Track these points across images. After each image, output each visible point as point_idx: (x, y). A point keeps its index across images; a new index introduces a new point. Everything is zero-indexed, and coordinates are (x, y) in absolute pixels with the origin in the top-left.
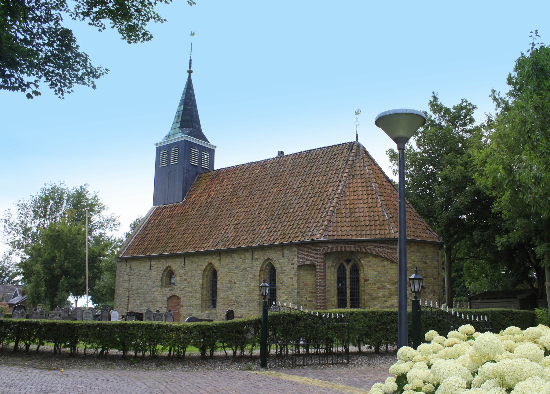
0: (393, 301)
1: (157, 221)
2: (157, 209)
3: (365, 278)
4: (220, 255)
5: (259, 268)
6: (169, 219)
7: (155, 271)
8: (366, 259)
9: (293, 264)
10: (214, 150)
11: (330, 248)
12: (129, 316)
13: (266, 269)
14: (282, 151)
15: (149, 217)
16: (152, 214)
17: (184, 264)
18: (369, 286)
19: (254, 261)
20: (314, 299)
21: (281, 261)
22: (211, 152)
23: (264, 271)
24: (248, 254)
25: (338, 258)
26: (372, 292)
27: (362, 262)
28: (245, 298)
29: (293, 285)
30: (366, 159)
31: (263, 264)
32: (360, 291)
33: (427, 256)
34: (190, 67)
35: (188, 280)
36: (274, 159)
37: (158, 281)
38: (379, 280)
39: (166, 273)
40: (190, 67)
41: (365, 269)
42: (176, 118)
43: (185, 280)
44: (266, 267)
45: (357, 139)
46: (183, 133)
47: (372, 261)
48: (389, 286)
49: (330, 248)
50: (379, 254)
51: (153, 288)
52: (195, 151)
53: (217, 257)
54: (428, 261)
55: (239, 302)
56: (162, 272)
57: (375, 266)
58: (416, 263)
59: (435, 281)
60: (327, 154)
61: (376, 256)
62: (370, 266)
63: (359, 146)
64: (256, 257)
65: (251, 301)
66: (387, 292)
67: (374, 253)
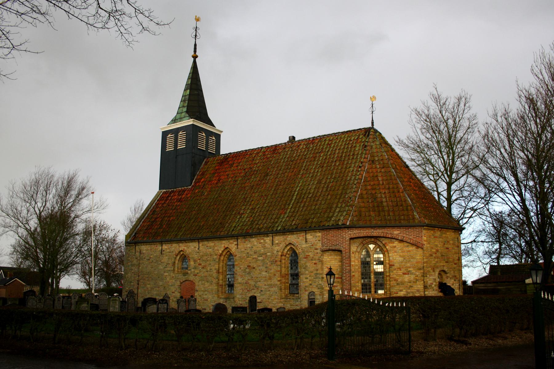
1: (165, 205)
2: (164, 193)
3: (391, 264)
5: (280, 254)
6: (179, 204)
7: (166, 256)
8: (391, 245)
9: (317, 249)
10: (220, 135)
12: (161, 303)
13: (287, 254)
14: (293, 137)
15: (156, 201)
16: (159, 197)
17: (198, 249)
18: (395, 272)
19: (274, 246)
20: (338, 284)
22: (218, 137)
23: (285, 256)
24: (268, 238)
25: (363, 244)
26: (398, 278)
27: (387, 247)
28: (265, 283)
30: (384, 145)
31: (284, 250)
33: (448, 242)
34: (195, 51)
35: (202, 265)
36: (285, 143)
37: (171, 265)
38: (405, 265)
39: (178, 257)
40: (195, 51)
41: (390, 255)
42: (182, 103)
43: (200, 264)
44: (287, 251)
46: (190, 117)
47: (397, 247)
48: (414, 271)
50: (404, 239)
51: (165, 272)
53: (234, 241)
55: (259, 287)
58: (439, 248)
59: (455, 266)
60: (342, 139)
61: (401, 241)
62: (395, 252)
63: (376, 131)
64: (277, 242)
65: (271, 286)
66: (412, 277)
67: (400, 239)
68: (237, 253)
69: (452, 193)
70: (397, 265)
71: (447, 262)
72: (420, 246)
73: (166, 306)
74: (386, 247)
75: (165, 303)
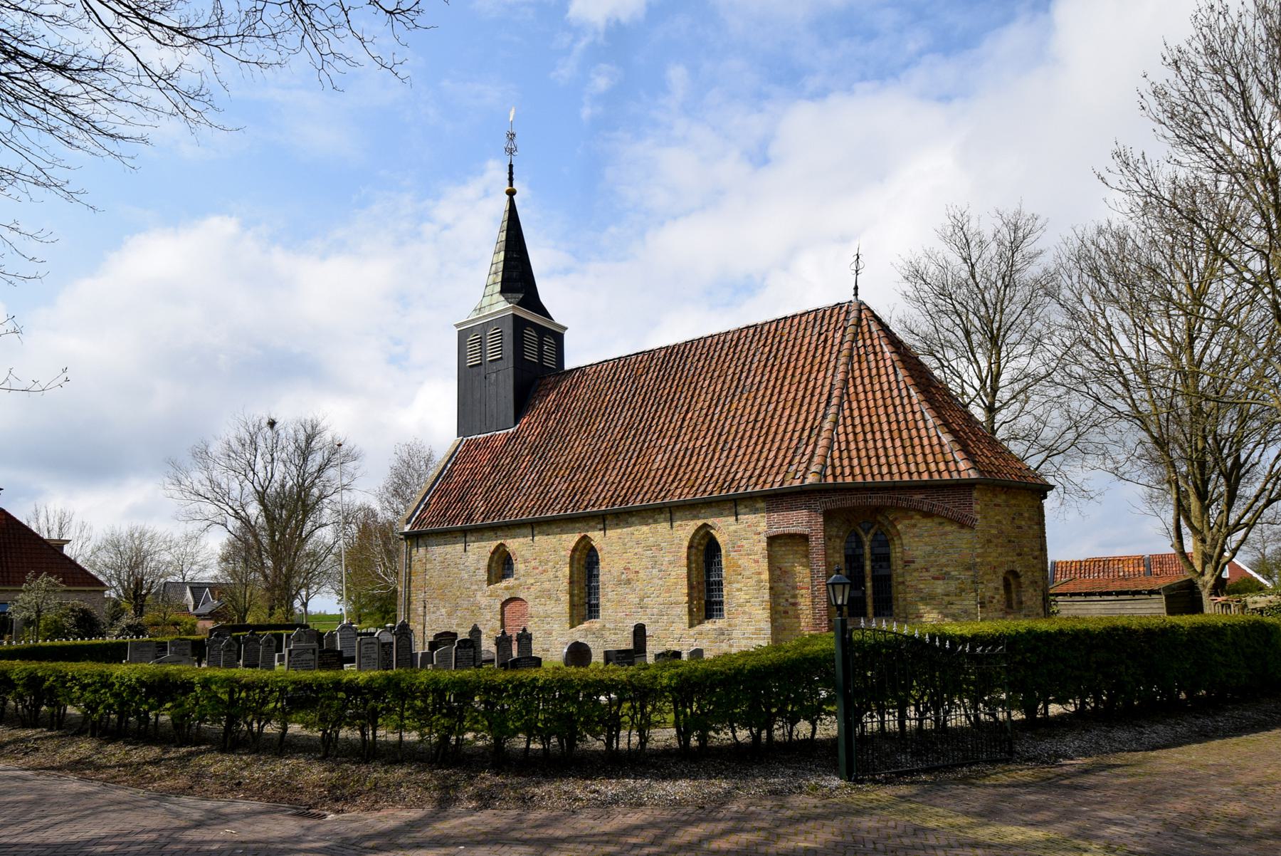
0: (967, 603)
4: (604, 521)
8: (907, 522)
10: (562, 335)
11: (834, 502)
13: (700, 544)
18: (916, 574)
21: (732, 528)
26: (922, 586)
27: (899, 527)
29: (760, 573)
32: (894, 584)
34: (511, 185)
38: (936, 561)
39: (496, 557)
41: (905, 541)
45: (856, 294)
47: (919, 525)
49: (834, 502)
52: (530, 333)
54: (1023, 523)
56: (489, 555)
57: (926, 534)
59: (1035, 561)
61: (928, 515)
63: (862, 307)
66: (953, 586)
67: (925, 509)
68: (604, 546)
69: (996, 426)
70: (920, 563)
71: (1019, 555)
72: (969, 522)
73: (472, 653)
74: (895, 527)
75: (470, 647)
